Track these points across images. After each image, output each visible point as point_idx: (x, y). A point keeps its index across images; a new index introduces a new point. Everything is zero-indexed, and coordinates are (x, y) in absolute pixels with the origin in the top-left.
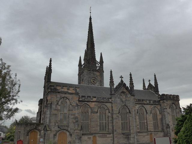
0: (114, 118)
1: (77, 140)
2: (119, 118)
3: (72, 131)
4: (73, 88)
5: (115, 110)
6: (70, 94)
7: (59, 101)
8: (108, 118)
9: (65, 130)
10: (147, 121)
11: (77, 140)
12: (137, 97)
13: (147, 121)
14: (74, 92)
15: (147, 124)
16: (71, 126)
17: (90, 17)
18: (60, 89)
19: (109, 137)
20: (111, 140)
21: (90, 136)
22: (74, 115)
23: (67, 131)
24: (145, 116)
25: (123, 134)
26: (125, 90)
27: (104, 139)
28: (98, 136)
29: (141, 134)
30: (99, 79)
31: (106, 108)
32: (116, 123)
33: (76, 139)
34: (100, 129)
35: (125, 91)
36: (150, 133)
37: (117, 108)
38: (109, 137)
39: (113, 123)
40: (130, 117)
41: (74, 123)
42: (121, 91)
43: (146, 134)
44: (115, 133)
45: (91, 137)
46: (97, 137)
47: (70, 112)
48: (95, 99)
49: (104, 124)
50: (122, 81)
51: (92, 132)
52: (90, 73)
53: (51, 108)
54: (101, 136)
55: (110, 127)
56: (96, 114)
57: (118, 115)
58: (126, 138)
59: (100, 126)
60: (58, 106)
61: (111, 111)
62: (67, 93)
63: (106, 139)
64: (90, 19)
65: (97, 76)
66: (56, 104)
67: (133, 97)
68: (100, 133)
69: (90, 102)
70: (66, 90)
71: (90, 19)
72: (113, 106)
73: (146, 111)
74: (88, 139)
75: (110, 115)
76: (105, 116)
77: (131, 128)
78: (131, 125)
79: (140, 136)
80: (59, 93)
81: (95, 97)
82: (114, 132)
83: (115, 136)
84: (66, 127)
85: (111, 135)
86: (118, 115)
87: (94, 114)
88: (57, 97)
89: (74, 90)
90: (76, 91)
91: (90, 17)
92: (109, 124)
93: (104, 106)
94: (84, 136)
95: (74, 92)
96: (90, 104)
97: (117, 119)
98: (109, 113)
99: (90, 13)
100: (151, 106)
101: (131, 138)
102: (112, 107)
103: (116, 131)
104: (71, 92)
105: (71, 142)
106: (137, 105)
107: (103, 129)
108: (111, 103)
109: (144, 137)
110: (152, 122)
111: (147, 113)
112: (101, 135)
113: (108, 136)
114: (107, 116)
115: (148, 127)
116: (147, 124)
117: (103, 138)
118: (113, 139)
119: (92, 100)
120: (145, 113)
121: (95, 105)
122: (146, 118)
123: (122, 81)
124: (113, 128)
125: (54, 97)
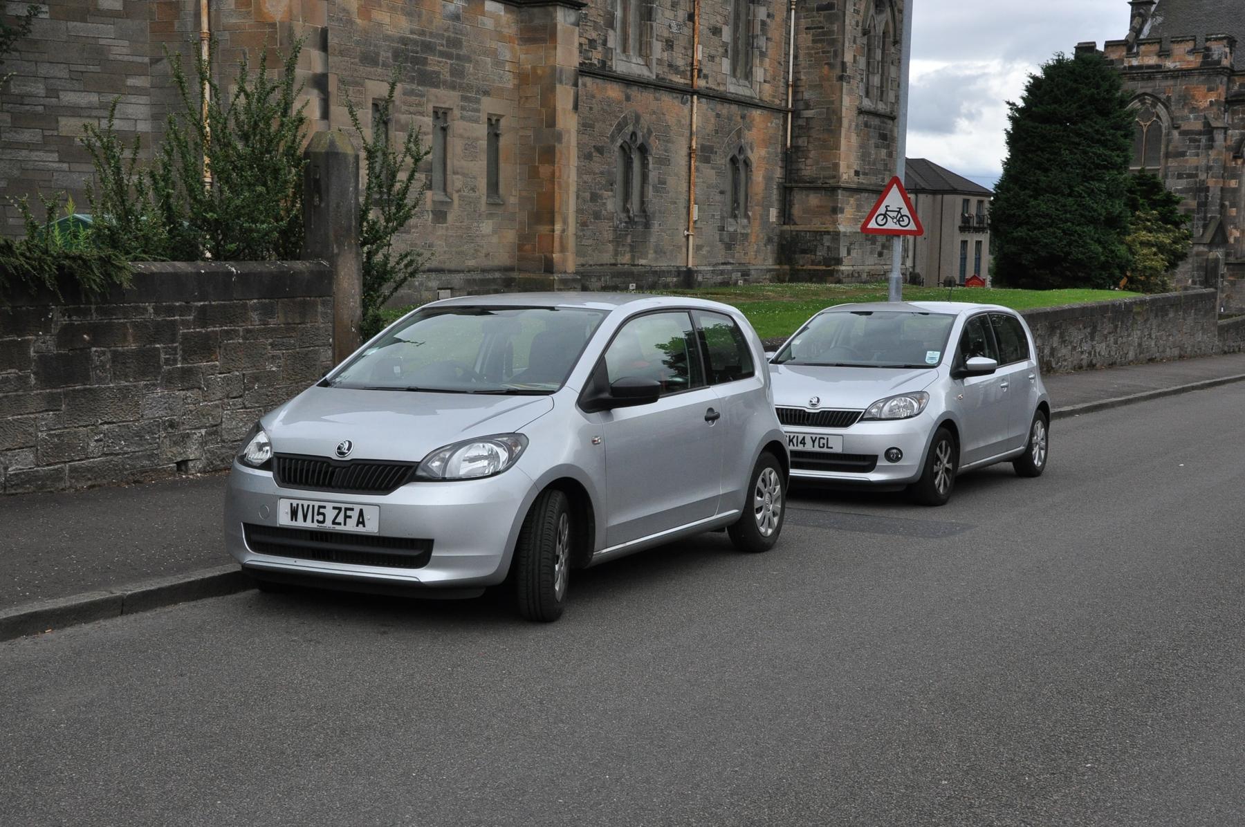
4: (1190, 45)
6: (1173, 77)
18: (1122, 61)
22: (1190, 176)
47: (1172, 163)
50: (778, 372)
53: (386, 123)
70: (1152, 60)
89: (1192, 52)
90: (1206, 56)
95: (1194, 61)
104: (1178, 65)
123: (778, 372)
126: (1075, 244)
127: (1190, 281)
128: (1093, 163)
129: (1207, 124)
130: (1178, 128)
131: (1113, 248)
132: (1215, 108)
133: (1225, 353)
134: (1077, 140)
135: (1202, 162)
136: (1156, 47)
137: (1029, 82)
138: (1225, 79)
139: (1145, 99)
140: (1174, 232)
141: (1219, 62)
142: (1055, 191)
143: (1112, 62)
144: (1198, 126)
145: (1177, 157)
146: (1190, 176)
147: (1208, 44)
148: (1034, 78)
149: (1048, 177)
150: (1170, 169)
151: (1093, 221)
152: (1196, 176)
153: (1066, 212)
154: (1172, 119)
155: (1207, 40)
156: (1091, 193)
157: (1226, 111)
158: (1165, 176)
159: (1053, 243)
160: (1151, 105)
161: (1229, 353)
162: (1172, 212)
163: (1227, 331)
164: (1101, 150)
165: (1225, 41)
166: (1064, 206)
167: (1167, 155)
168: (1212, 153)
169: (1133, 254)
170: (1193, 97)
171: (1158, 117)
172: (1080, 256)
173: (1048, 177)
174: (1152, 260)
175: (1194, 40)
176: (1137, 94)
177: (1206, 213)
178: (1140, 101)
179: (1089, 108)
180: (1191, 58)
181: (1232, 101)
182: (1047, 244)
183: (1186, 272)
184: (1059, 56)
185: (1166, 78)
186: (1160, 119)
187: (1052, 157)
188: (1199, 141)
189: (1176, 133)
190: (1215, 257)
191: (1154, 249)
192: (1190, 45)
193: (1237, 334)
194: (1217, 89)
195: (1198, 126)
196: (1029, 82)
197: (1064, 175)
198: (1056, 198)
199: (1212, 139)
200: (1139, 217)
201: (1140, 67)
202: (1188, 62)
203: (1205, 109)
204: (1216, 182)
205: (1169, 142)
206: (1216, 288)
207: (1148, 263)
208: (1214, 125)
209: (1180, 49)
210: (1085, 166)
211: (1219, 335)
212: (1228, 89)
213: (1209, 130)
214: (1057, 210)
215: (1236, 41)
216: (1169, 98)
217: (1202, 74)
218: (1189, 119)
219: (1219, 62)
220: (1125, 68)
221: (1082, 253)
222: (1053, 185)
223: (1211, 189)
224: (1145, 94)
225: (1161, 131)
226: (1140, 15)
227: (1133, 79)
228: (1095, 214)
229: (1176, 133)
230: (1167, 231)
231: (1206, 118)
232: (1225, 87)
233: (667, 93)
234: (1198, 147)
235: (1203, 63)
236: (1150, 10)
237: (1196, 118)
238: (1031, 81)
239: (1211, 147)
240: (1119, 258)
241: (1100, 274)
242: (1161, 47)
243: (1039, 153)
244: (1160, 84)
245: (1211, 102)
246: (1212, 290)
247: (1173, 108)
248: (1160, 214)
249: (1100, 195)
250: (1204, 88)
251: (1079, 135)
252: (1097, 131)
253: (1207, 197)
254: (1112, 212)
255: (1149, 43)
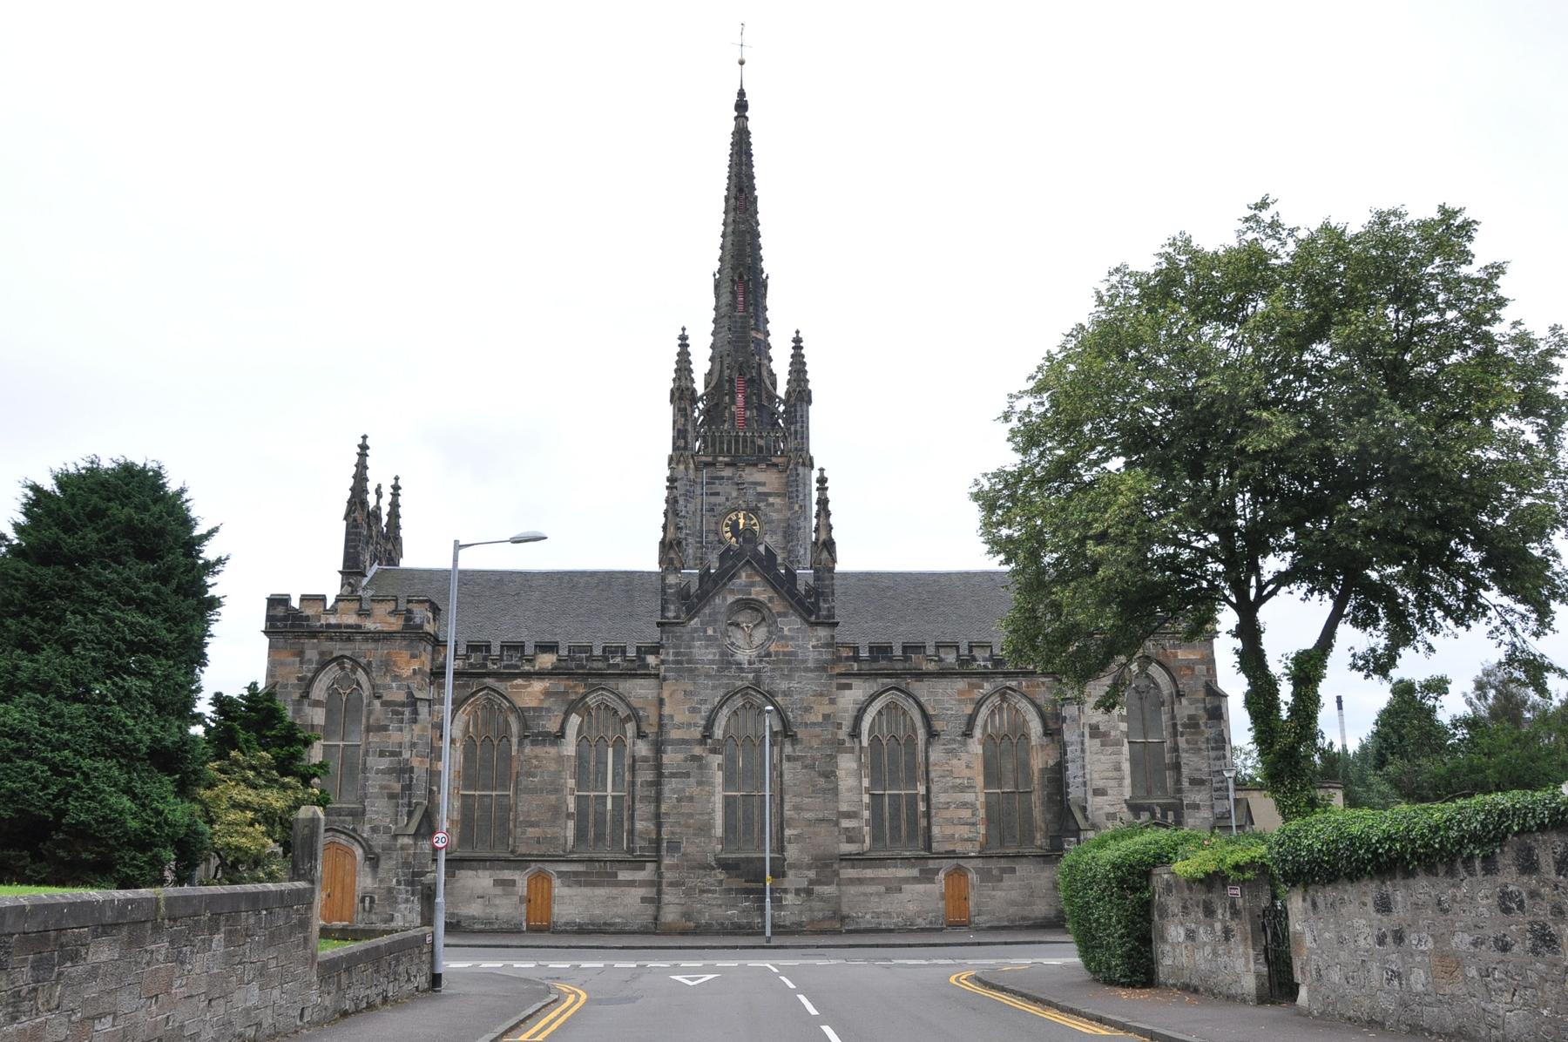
0: (666, 772)
1: (402, 887)
2: (701, 767)
3: (379, 841)
4: (391, 606)
5: (678, 719)
7: (312, 680)
8: (633, 771)
9: (343, 837)
10: (928, 789)
11: (402, 887)
12: (859, 631)
13: (928, 789)
14: (394, 628)
15: (928, 806)
16: (377, 812)
17: (741, 93)
18: (318, 618)
19: (631, 883)
20: (644, 900)
21: (507, 875)
22: (393, 754)
23: (353, 838)
24: (921, 757)
25: (725, 865)
26: (761, 593)
27: (601, 892)
28: (561, 874)
29: (869, 873)
30: (775, 516)
31: (623, 712)
32: (679, 800)
33: (399, 883)
34: (581, 835)
35: (763, 597)
36: (948, 864)
37: (693, 710)
38: (631, 883)
39: (658, 800)
40: (786, 765)
41: (392, 796)
42: (730, 599)
43: (915, 872)
44: (667, 861)
45: (521, 879)
46: (556, 882)
47: (374, 738)
48: (547, 660)
49: (609, 806)
51: (522, 849)
52: (713, 480)
54: (576, 874)
55: (639, 825)
56: (552, 751)
57: (697, 750)
58: (748, 891)
59: (581, 816)
60: (307, 709)
61: (650, 730)
62: (359, 637)
63: (614, 891)
64: (742, 106)
65: (769, 494)
66: (296, 696)
67: (823, 633)
68: (575, 856)
69: (516, 676)
70: (352, 619)
71: (742, 106)
72: (665, 695)
73: (927, 718)
74: (498, 891)
75: (643, 749)
76: (618, 756)
77: (787, 832)
78: (788, 813)
79: (860, 881)
80: (313, 634)
81: (550, 648)
82: (664, 853)
83: (668, 876)
84: (349, 819)
85: (647, 873)
86: (697, 750)
87: (539, 750)
88: (302, 662)
89: (394, 612)
91: (741, 93)
92: (638, 805)
93: (613, 702)
94: (470, 873)
95: (396, 624)
96: (512, 687)
97: (688, 775)
98: (639, 742)
99: (742, 63)
100: (972, 686)
101: (785, 891)
102: (661, 702)
103: (674, 847)
104: (379, 627)
105: (372, 901)
106: (855, 682)
107: (599, 837)
108: (657, 676)
109: (893, 887)
110: (977, 797)
111: (932, 734)
112: (580, 868)
113: (623, 875)
114: (627, 761)
115: (935, 830)
116: (928, 806)
117: (593, 884)
118: (659, 892)
119: (527, 668)
120: (921, 734)
121: (548, 693)
122: (923, 768)
124: (659, 833)
125: (292, 659)
126: (75, 793)
127: (394, 880)
128: (124, 640)
129: (410, 695)
130: (379, 697)
131: (161, 807)
132: (419, 677)
133: (345, 1014)
134: (95, 594)
135: (406, 738)
136: (356, 605)
137: (26, 495)
138: (429, 648)
139: (344, 663)
140: (295, 789)
141: (421, 626)
142: (45, 687)
143: (307, 618)
144: (400, 696)
145: (379, 731)
146: (393, 754)
147: (410, 606)
148: (36, 489)
149: (36, 661)
150: (372, 745)
151: (125, 754)
152: (400, 753)
153: (62, 728)
154: (373, 687)
155: (409, 601)
156: (125, 697)
157: (431, 683)
158: (367, 753)
159: (26, 791)
160: (351, 670)
161: (358, 1011)
162: (295, 757)
163: (348, 970)
164: (138, 618)
165: (427, 604)
166: (60, 716)
167: (368, 729)
168: (417, 728)
169: (211, 822)
170: (395, 663)
171: (358, 684)
172: (83, 817)
173: (36, 661)
174: (245, 834)
175: (396, 600)
176: (334, 655)
177: (410, 797)
178: (338, 664)
179: (121, 542)
180: (392, 620)
181: (436, 673)
182: (13, 791)
183: (390, 870)
184: (92, 462)
185: (366, 640)
186: (361, 688)
187: (47, 627)
188: (403, 714)
189: (377, 703)
190: (310, 815)
191: (250, 814)
192: (391, 606)
193: (377, 971)
194: (420, 656)
195: (400, 696)
196: (26, 495)
197: (67, 660)
198: (46, 701)
199: (415, 712)
200: (236, 762)
201: (339, 626)
202: (390, 624)
203: (408, 678)
204: (421, 762)
205: (370, 713)
206: (312, 882)
207: (236, 840)
208: (418, 695)
209: (381, 610)
210: (109, 645)
211: (323, 980)
212: (433, 660)
213: (413, 702)
214: (43, 723)
215: (440, 610)
216: (370, 663)
217: (404, 638)
218: (392, 688)
219: (421, 626)
220: (322, 626)
221: (88, 810)
222: (41, 676)
223: (415, 770)
224: (343, 656)
225: (362, 701)
226: (350, 584)
227: (331, 639)
228: (130, 740)
229: (377, 703)
230: (284, 787)
231: (409, 688)
232: (429, 657)
233: (485, 869)
234: (402, 721)
235: (406, 626)
236: (360, 582)
237: (399, 688)
238: (30, 494)
239: (415, 721)
240: (170, 825)
241: (133, 858)
242: (361, 606)
243: (25, 618)
244: (360, 647)
245: (414, 670)
246: (301, 885)
247: (374, 675)
248: (274, 757)
249: (143, 703)
250: (406, 654)
251: (99, 586)
252: (127, 581)
253: (411, 779)
254: (163, 739)
255: (348, 600)
